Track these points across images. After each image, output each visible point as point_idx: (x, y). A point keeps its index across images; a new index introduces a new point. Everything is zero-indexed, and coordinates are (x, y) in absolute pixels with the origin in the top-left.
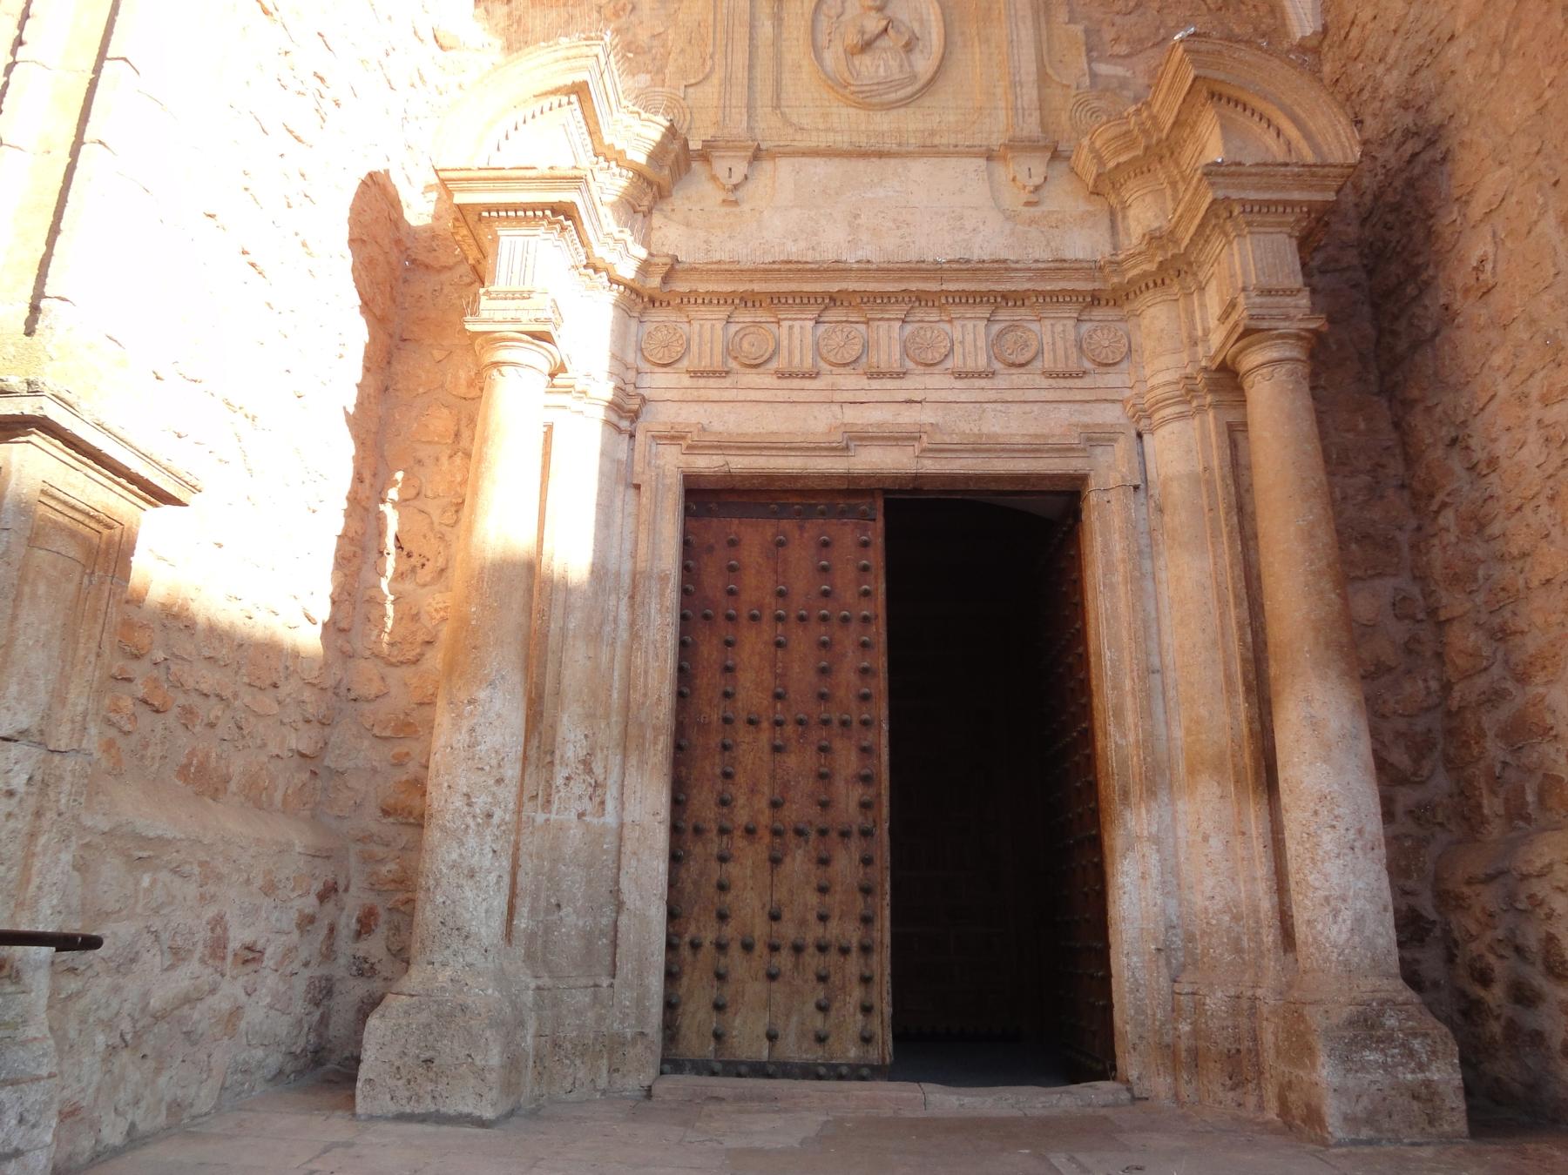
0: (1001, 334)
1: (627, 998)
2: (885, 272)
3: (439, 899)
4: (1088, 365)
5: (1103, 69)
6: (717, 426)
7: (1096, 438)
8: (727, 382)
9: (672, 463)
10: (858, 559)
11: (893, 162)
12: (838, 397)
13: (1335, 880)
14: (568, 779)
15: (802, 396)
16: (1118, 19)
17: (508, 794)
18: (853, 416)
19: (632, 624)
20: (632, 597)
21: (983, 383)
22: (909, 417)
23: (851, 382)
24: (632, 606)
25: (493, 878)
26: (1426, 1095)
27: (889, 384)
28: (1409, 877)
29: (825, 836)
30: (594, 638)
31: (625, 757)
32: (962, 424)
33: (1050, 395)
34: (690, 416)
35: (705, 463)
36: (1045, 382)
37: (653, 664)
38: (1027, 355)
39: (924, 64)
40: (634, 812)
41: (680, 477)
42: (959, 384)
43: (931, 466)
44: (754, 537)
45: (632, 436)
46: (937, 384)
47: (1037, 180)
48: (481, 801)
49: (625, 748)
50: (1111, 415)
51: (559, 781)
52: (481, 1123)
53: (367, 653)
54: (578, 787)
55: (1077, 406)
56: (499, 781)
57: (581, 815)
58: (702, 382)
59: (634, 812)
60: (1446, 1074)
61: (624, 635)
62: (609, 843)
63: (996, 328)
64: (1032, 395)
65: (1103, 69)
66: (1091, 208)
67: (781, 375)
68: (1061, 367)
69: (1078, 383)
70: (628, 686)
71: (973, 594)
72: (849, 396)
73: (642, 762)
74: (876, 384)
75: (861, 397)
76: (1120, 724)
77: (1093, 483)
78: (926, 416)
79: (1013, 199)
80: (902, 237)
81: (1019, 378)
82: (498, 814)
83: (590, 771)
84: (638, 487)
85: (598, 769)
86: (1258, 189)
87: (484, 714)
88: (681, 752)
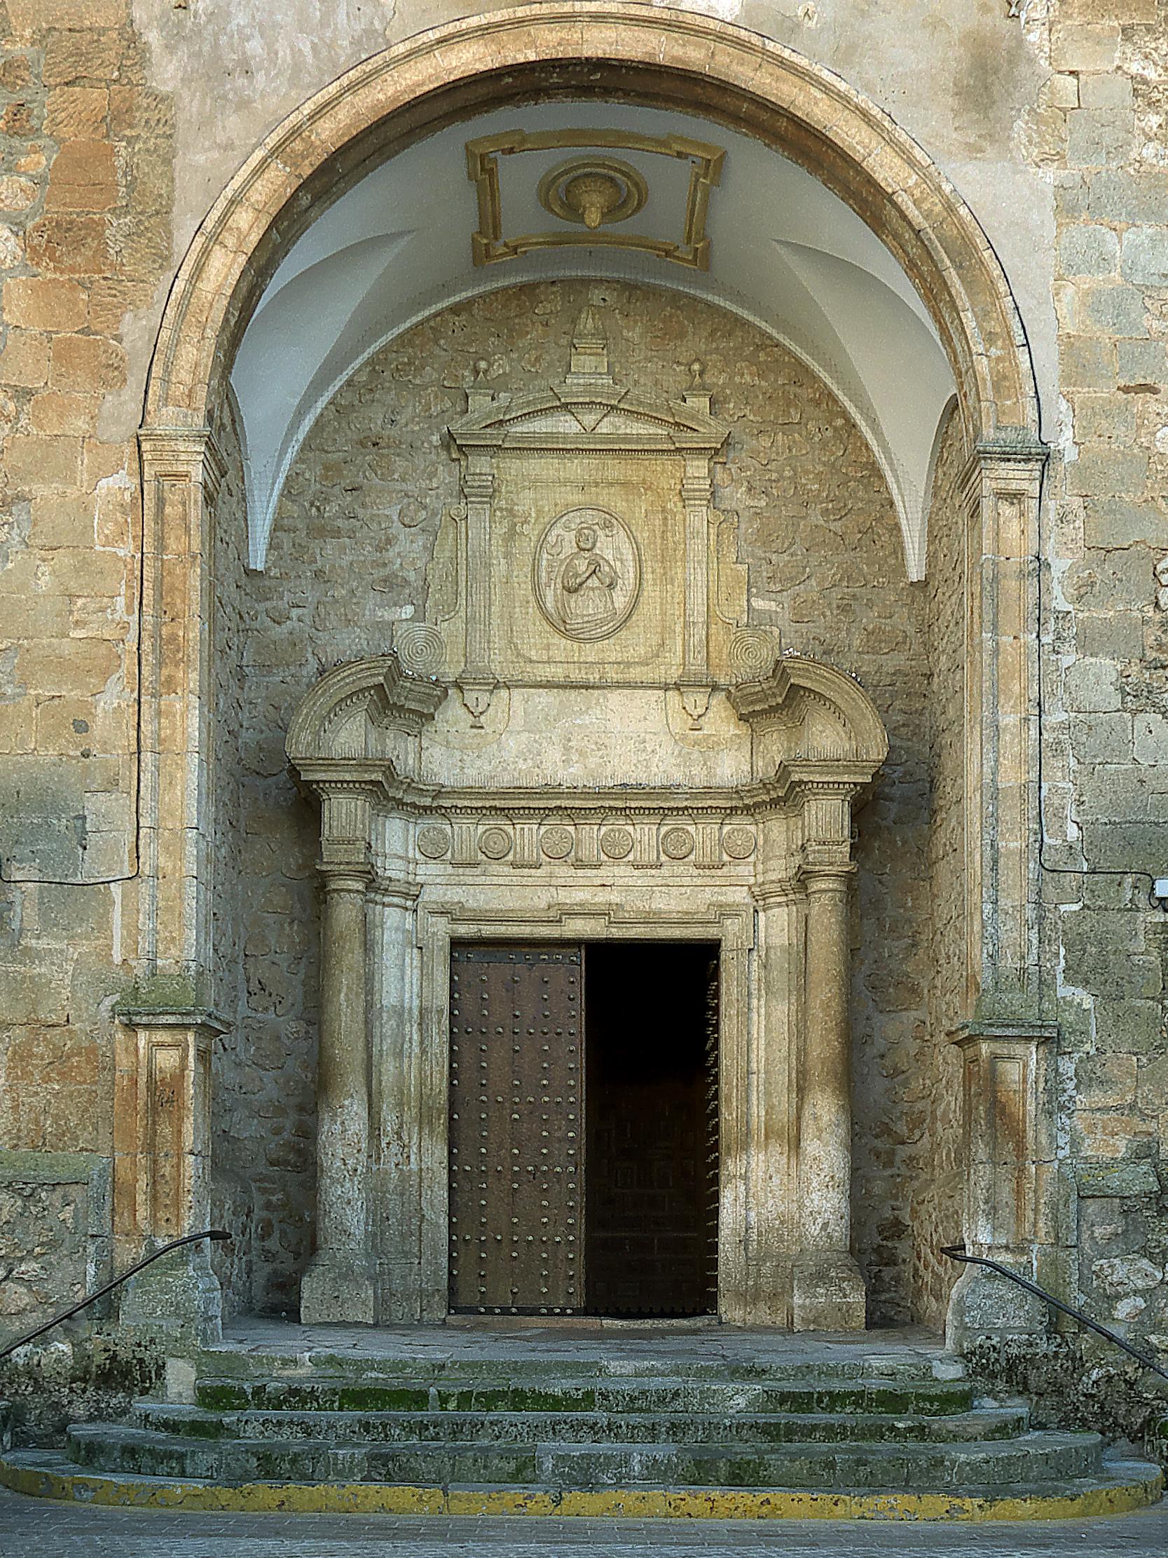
0: (666, 835)
1: (428, 1270)
2: (587, 794)
3: (333, 1215)
4: (726, 858)
5: (758, 604)
6: (471, 904)
7: (725, 912)
8: (478, 871)
9: (442, 929)
10: (569, 983)
11: (596, 692)
12: (554, 882)
13: (816, 1202)
14: (388, 1144)
15: (530, 881)
16: (774, 557)
17: (363, 1157)
18: (564, 897)
19: (422, 1043)
20: (420, 1024)
21: (653, 872)
22: (602, 897)
23: (564, 872)
24: (421, 1030)
25: (359, 1203)
26: (845, 1311)
27: (590, 872)
28: (897, 1199)
29: (1149, 214)
30: (399, 1054)
31: (420, 1129)
32: (636, 903)
33: (699, 881)
34: (454, 895)
35: (463, 930)
36: (696, 872)
37: (436, 1069)
38: (685, 850)
39: (620, 600)
40: (427, 1161)
41: (448, 940)
42: (636, 872)
43: (616, 933)
44: (495, 973)
45: (415, 911)
46: (621, 873)
47: (700, 711)
48: (350, 1162)
49: (421, 1123)
50: (739, 896)
51: (384, 1145)
52: (367, 1326)
53: (250, 1063)
54: (394, 1149)
55: (716, 889)
56: (359, 1151)
57: (397, 1165)
58: (461, 871)
59: (427, 1161)
60: (857, 1298)
61: (417, 1050)
62: (414, 1180)
63: (664, 830)
64: (686, 881)
65: (758, 604)
66: (737, 732)
67: (514, 865)
68: (707, 861)
69: (719, 872)
70: (422, 1084)
71: (651, 1000)
72: (562, 882)
73: (431, 1131)
74: (580, 872)
75: (570, 882)
76: (728, 1107)
77: (723, 944)
78: (615, 897)
79: (679, 724)
80: (602, 757)
81: (679, 869)
82: (360, 1168)
83: (400, 1138)
84: (421, 948)
85: (405, 1137)
86: (821, 773)
87: (348, 1114)
88: (452, 1124)
